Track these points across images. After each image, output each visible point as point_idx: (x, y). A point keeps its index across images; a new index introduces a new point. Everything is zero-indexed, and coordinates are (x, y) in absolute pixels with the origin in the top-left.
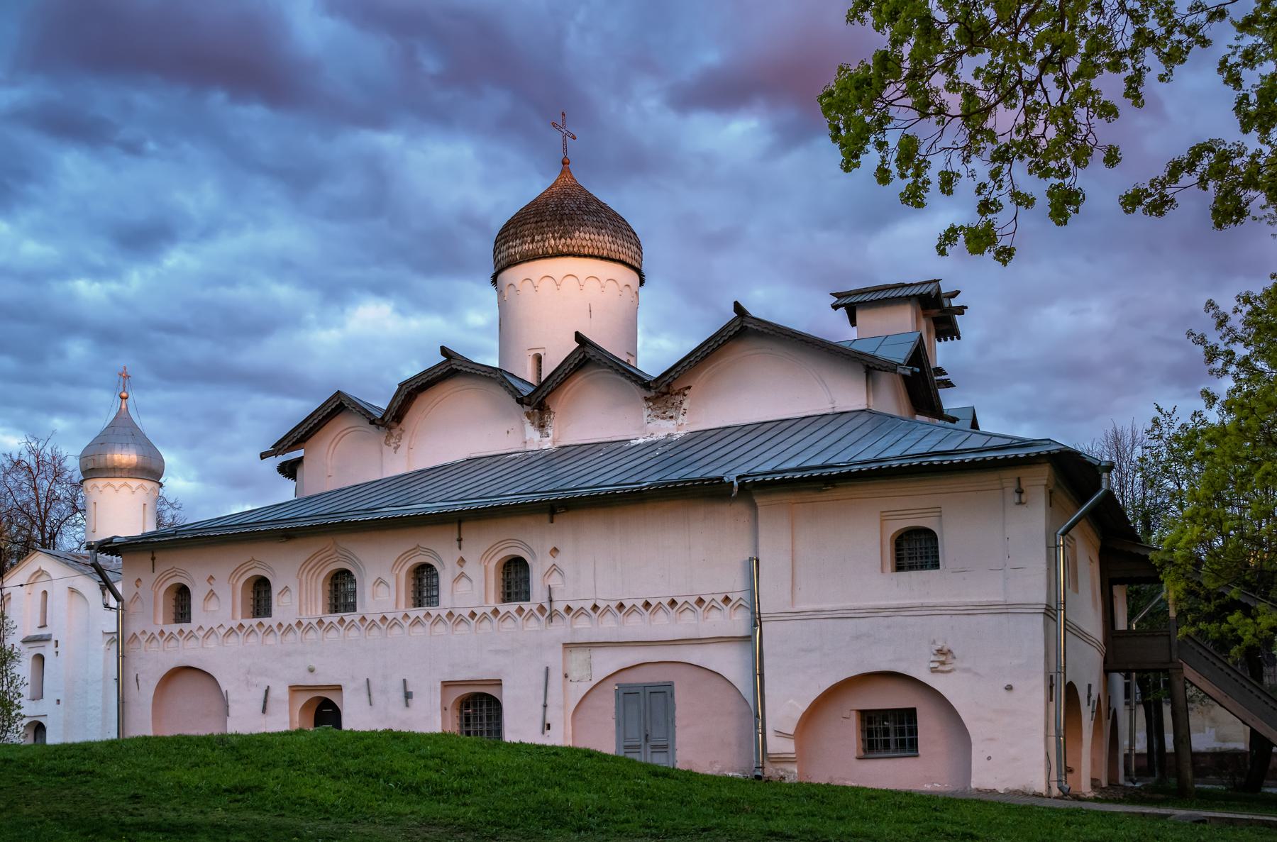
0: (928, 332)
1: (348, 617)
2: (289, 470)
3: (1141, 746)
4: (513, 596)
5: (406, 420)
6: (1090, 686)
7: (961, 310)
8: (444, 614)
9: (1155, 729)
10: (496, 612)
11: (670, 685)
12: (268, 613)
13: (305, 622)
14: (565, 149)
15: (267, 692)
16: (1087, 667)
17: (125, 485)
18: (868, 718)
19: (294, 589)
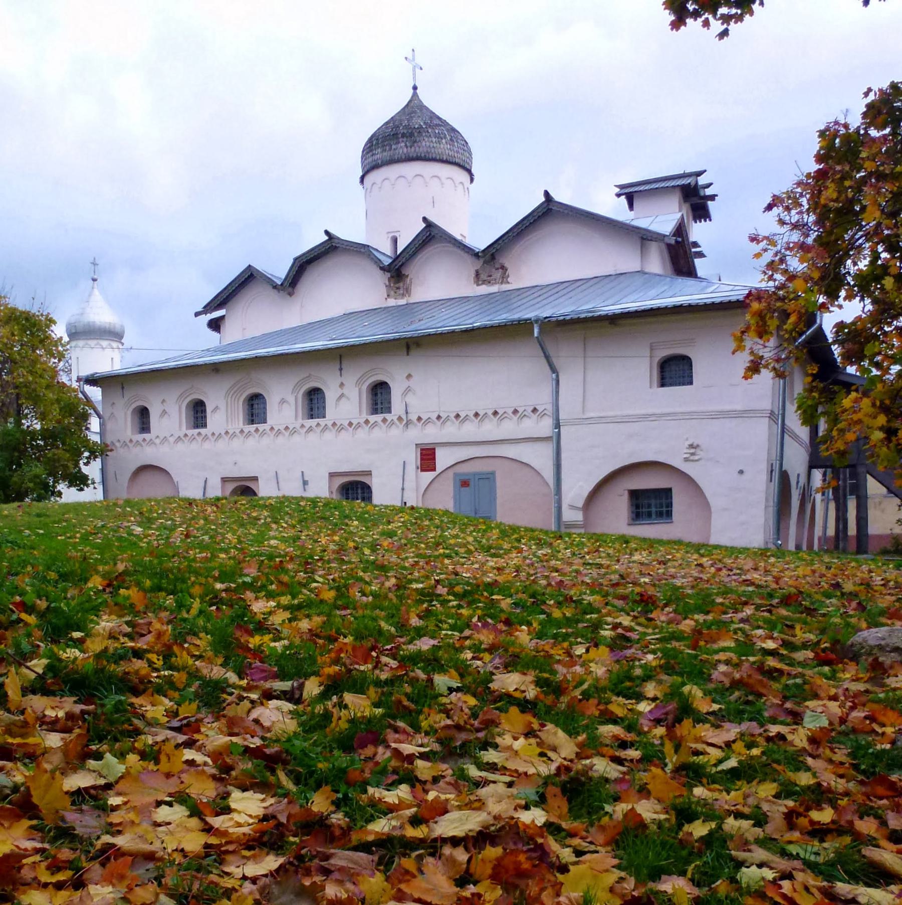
0: (687, 213)
1: (261, 427)
2: (215, 325)
3: (831, 532)
4: (379, 410)
5: (299, 286)
6: (798, 475)
7: (712, 198)
8: (330, 423)
9: (841, 519)
10: (367, 422)
11: (493, 474)
12: (204, 425)
13: (231, 432)
14: (414, 78)
15: (206, 481)
16: (796, 459)
17: (98, 344)
18: (635, 496)
19: (223, 407)
